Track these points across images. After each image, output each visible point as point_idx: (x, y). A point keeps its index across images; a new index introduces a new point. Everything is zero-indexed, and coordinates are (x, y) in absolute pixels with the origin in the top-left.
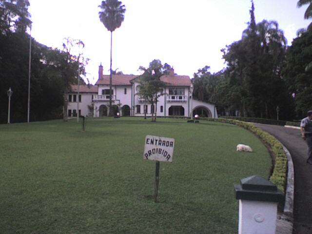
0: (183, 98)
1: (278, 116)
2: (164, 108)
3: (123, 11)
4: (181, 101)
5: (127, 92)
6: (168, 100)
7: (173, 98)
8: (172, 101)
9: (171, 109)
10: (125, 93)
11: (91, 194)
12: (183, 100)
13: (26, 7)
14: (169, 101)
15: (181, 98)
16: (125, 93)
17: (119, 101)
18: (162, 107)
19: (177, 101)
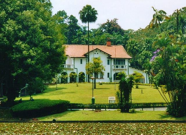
0: (124, 67)
1: (35, 97)
2: (110, 74)
3: (84, 7)
4: (118, 69)
5: (82, 62)
6: (113, 68)
7: (117, 67)
8: (122, 69)
9: (116, 74)
10: (81, 63)
11: (164, 127)
12: (124, 68)
13: (57, 14)
14: (114, 69)
15: (122, 67)
16: (81, 63)
17: (77, 69)
18: (108, 74)
19: (120, 69)
